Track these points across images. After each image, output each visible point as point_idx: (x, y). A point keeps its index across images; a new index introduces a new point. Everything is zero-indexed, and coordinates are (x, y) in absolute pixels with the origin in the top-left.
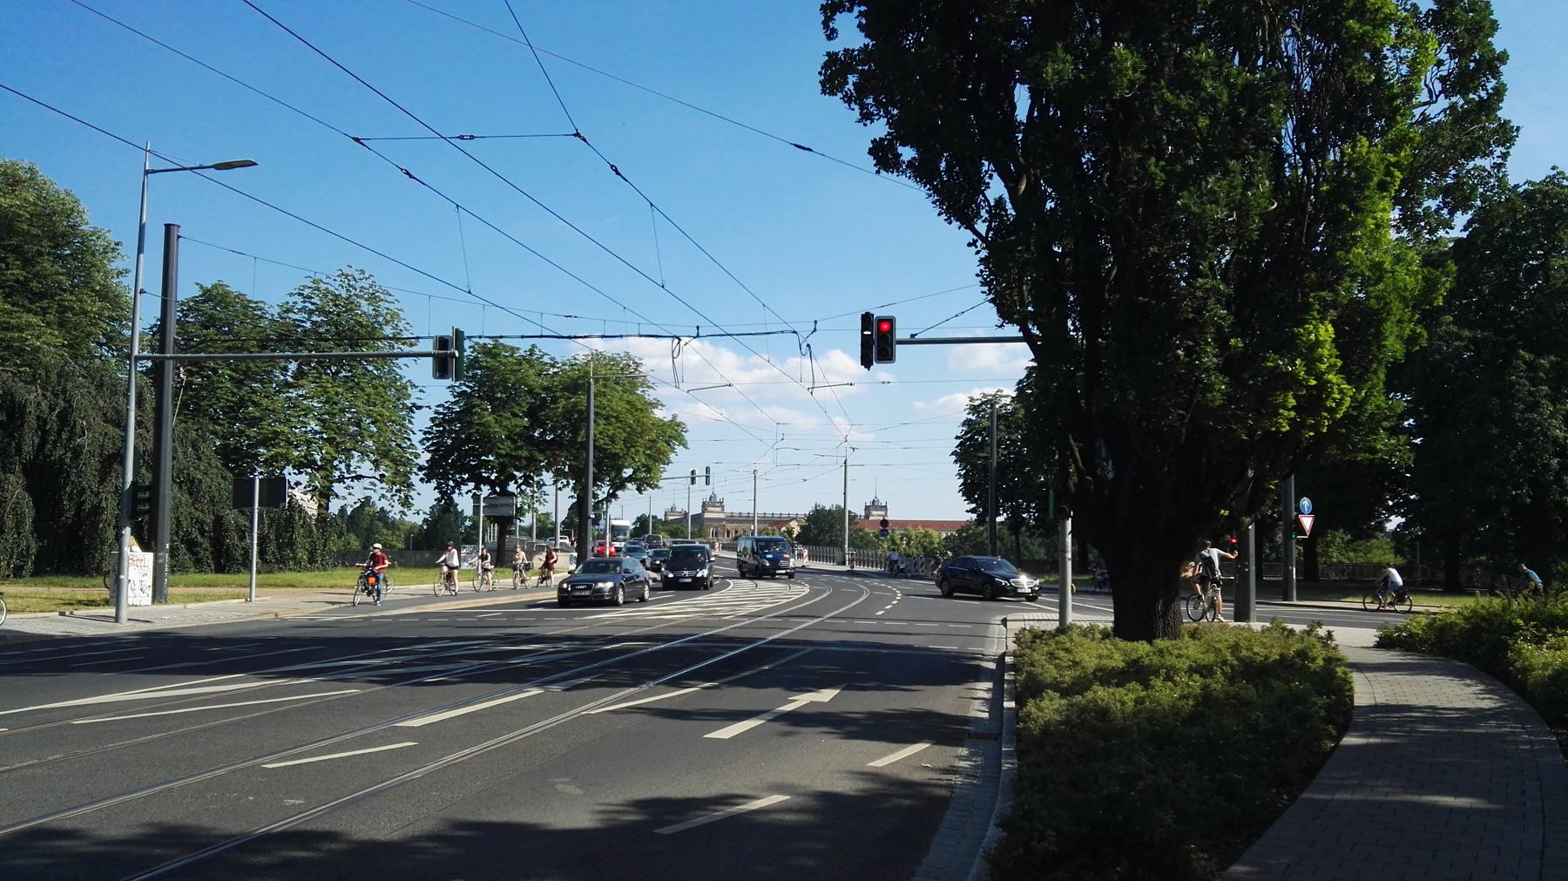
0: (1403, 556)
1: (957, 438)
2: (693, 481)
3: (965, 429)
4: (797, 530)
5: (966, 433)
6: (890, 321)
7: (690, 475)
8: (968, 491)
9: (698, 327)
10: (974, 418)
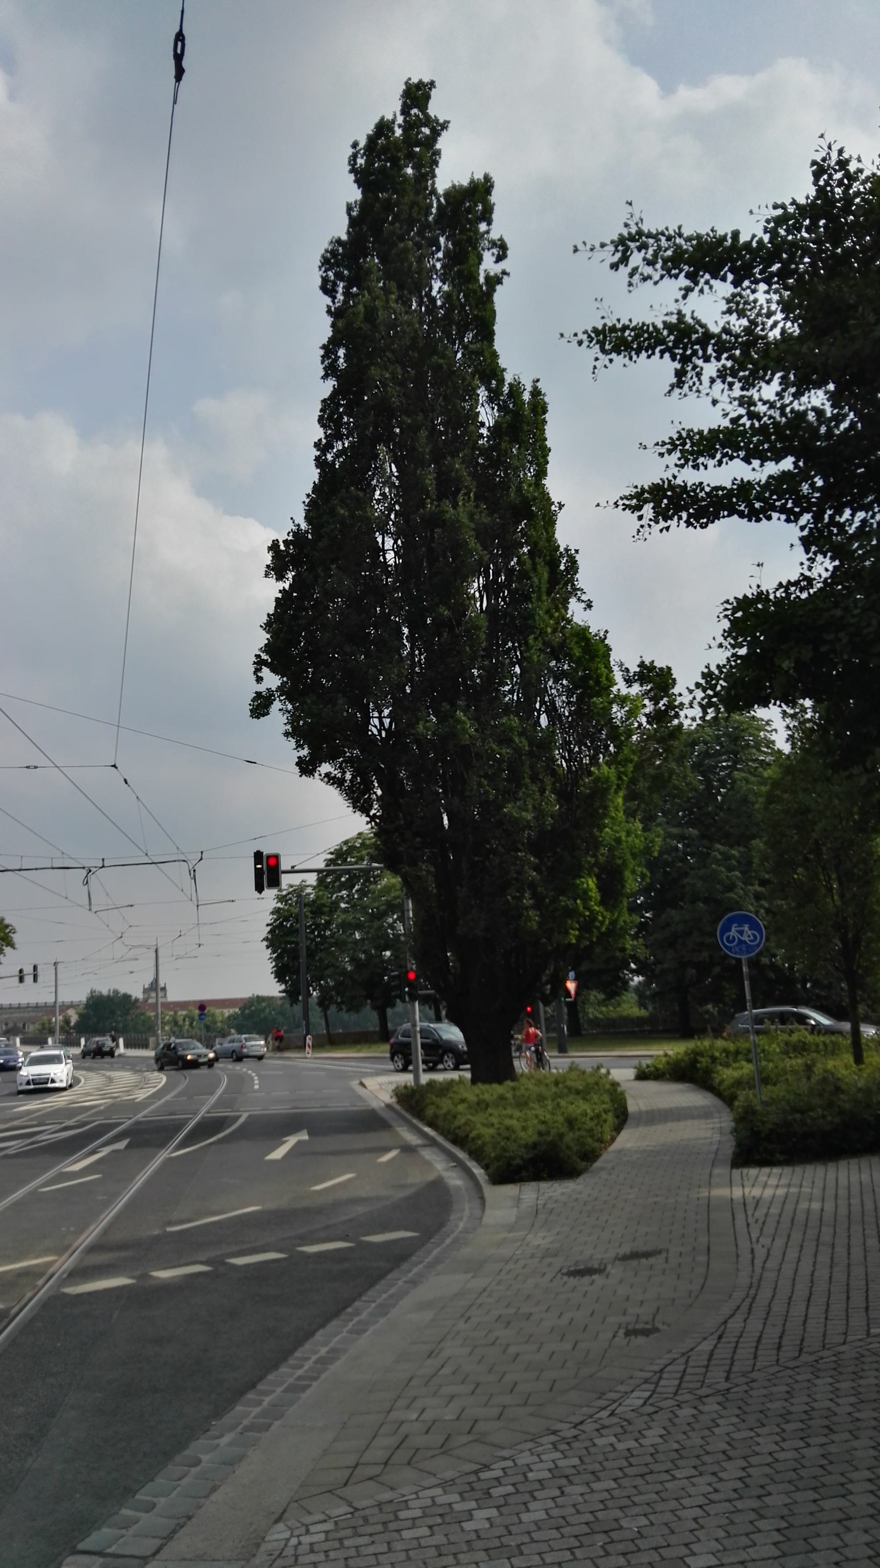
0: (646, 1008)
1: (268, 925)
2: (21, 980)
3: (275, 917)
4: (74, 1019)
5: (276, 920)
6: (276, 857)
7: (17, 973)
8: (280, 974)
9: (103, 860)
10: (282, 906)
